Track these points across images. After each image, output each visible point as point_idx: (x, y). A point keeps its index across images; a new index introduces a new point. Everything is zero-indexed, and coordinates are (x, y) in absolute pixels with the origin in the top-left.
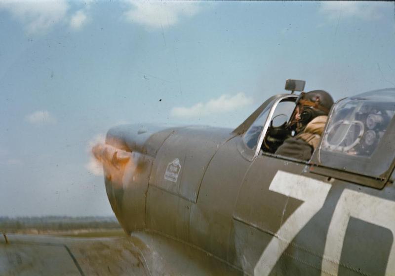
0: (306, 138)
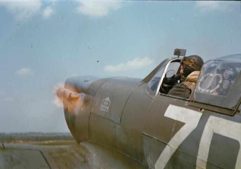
0: (187, 85)
